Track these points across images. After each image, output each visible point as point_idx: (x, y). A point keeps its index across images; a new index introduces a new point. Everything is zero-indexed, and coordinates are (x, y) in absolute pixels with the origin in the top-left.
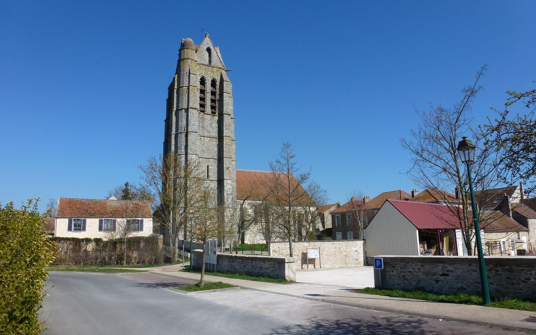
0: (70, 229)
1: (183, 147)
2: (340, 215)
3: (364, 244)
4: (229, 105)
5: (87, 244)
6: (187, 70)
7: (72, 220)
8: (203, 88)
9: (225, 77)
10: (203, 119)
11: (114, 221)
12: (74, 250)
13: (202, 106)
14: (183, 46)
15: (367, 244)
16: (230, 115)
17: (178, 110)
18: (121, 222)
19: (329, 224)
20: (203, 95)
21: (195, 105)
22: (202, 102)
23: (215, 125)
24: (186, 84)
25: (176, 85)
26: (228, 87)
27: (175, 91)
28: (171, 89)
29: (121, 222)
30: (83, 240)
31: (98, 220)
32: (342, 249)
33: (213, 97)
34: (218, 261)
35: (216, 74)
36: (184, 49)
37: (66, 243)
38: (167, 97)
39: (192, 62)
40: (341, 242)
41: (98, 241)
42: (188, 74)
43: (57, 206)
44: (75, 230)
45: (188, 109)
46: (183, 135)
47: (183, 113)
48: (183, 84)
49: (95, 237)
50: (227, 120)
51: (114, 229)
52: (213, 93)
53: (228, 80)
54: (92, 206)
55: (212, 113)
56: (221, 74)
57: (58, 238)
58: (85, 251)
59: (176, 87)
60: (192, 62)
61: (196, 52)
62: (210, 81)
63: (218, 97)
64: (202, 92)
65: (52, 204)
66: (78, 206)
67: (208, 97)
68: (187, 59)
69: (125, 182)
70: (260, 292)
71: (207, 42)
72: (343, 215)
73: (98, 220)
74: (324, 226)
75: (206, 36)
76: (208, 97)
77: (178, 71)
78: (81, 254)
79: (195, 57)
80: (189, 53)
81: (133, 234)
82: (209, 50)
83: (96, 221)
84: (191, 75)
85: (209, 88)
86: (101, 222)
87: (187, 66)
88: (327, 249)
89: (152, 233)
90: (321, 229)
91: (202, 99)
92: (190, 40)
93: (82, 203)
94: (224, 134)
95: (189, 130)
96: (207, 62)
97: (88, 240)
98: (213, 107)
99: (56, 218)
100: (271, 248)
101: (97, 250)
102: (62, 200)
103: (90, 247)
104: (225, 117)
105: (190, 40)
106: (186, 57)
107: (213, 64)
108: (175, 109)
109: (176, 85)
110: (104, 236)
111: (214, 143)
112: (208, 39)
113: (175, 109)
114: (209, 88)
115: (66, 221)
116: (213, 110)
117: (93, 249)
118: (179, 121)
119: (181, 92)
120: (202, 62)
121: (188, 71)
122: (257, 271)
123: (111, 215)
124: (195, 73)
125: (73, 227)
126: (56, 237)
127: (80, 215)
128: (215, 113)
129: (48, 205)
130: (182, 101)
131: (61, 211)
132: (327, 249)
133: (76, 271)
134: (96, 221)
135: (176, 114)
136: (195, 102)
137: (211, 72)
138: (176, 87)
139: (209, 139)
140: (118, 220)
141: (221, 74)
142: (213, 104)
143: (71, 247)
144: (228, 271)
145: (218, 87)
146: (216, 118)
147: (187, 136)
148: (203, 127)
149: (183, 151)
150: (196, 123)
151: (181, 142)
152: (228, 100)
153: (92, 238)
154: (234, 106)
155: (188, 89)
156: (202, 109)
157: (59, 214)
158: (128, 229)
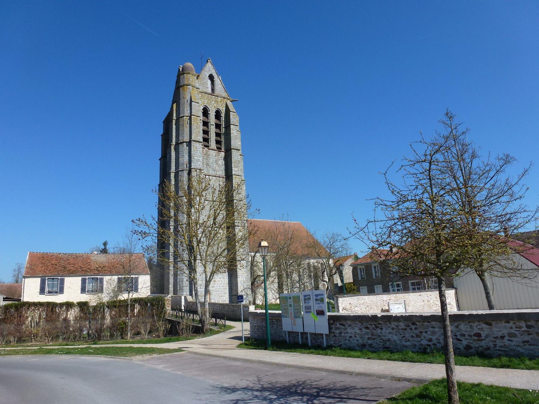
0: (42, 291)
2: (363, 267)
3: (456, 293)
4: (236, 141)
5: (68, 311)
7: (45, 280)
8: (206, 120)
9: (231, 108)
10: (207, 155)
11: (102, 280)
12: (49, 320)
13: (206, 140)
14: (181, 74)
15: (459, 292)
16: (239, 150)
17: (178, 144)
18: (110, 281)
19: (348, 277)
20: (206, 128)
21: (199, 137)
22: (206, 136)
23: (222, 162)
24: (187, 113)
25: (175, 115)
26: (234, 118)
27: (174, 122)
28: (167, 122)
29: (110, 281)
30: (61, 305)
31: (80, 279)
32: (431, 302)
33: (218, 131)
34: (330, 328)
37: (39, 310)
38: (161, 132)
39: (193, 89)
40: (366, 297)
41: (83, 305)
42: (189, 102)
43: (23, 271)
44: (49, 292)
45: (190, 142)
46: (185, 173)
47: (184, 148)
49: (79, 301)
50: (236, 156)
51: (101, 291)
52: (218, 126)
53: (234, 110)
54: (72, 261)
55: (218, 148)
56: (226, 104)
57: (27, 303)
58: (66, 320)
59: (174, 117)
60: (193, 89)
61: (197, 78)
63: (223, 130)
64: (205, 124)
65: (19, 269)
66: (54, 262)
67: (213, 130)
68: (188, 85)
69: (103, 241)
71: (209, 69)
72: (368, 267)
73: (80, 279)
74: (342, 281)
75: (207, 62)
76: (213, 130)
77: (177, 99)
78: (59, 324)
79: (197, 83)
80: (190, 78)
81: (124, 296)
82: (211, 77)
83: (77, 281)
84: (193, 103)
85: (212, 120)
86: (84, 282)
87: (187, 94)
88: (413, 303)
89: (149, 294)
90: (340, 284)
91: (206, 132)
92: (189, 64)
93: (58, 258)
94: (233, 172)
95: (193, 167)
96: (210, 91)
97: (69, 305)
98: (218, 142)
99: (24, 277)
100: (340, 304)
101: (81, 317)
102: (32, 255)
103: (72, 314)
104: (234, 152)
105: (189, 64)
107: (217, 92)
108: (174, 142)
109: (175, 115)
110: (92, 300)
113: (174, 142)
114: (212, 120)
115: (38, 281)
116: (219, 146)
117: (76, 318)
118: (180, 156)
119: (181, 123)
120: (204, 90)
121: (189, 99)
122: (465, 343)
123: (97, 272)
124: (198, 101)
125: (47, 290)
126: (24, 302)
127: (56, 273)
128: (221, 149)
129: (15, 270)
130: (183, 133)
131: (31, 269)
132: (413, 303)
133: (57, 353)
134: (77, 281)
135: (175, 149)
136: (198, 134)
137: (215, 101)
138: (174, 117)
139: (214, 178)
140: (106, 278)
141: (226, 104)
142: (218, 138)
143: (44, 315)
144: (364, 346)
145: (223, 119)
146: (223, 154)
147: (189, 173)
148: (208, 165)
150: (201, 159)
152: (235, 132)
153: (75, 302)
154: (243, 140)
155: (190, 119)
156: (206, 143)
157: (27, 273)
158: (120, 290)
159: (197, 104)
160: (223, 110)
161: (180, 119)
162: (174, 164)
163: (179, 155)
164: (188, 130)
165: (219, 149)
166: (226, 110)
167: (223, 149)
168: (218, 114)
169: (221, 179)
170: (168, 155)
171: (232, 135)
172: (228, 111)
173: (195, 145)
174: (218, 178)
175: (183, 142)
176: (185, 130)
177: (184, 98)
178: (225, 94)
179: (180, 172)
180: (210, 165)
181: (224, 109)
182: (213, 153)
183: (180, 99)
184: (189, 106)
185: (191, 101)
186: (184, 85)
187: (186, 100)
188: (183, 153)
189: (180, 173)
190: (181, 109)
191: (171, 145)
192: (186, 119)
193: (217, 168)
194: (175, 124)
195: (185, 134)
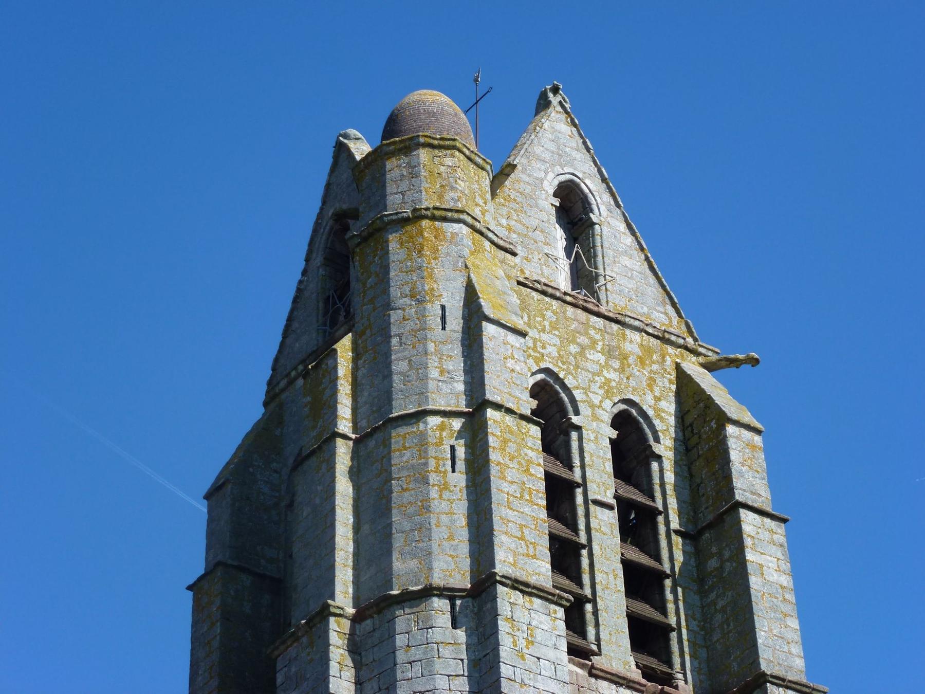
6: (452, 299)
17: (379, 607)
24: (448, 390)
35: (641, 375)
42: (455, 322)
52: (637, 524)
62: (607, 418)
63: (674, 554)
68: (442, 215)
70: (508, 246)
71: (555, 150)
82: (572, 210)
84: (489, 329)
92: (435, 99)
105: (435, 99)
106: (428, 201)
108: (344, 596)
114: (599, 476)
119: (402, 457)
121: (455, 304)
124: (520, 324)
130: (424, 530)
135: (354, 648)
137: (609, 352)
156: (581, 295)
159: (512, 338)
160: (663, 414)
161: (398, 435)
164: (461, 508)
166: (681, 416)
168: (630, 431)
171: (755, 582)
172: (701, 424)
173: (521, 615)
175: (428, 592)
176: (439, 505)
178: (662, 316)
181: (669, 406)
183: (388, 306)
184: (457, 350)
186: (418, 216)
190: (399, 366)
192: (443, 434)
194: (354, 474)
195: (439, 534)
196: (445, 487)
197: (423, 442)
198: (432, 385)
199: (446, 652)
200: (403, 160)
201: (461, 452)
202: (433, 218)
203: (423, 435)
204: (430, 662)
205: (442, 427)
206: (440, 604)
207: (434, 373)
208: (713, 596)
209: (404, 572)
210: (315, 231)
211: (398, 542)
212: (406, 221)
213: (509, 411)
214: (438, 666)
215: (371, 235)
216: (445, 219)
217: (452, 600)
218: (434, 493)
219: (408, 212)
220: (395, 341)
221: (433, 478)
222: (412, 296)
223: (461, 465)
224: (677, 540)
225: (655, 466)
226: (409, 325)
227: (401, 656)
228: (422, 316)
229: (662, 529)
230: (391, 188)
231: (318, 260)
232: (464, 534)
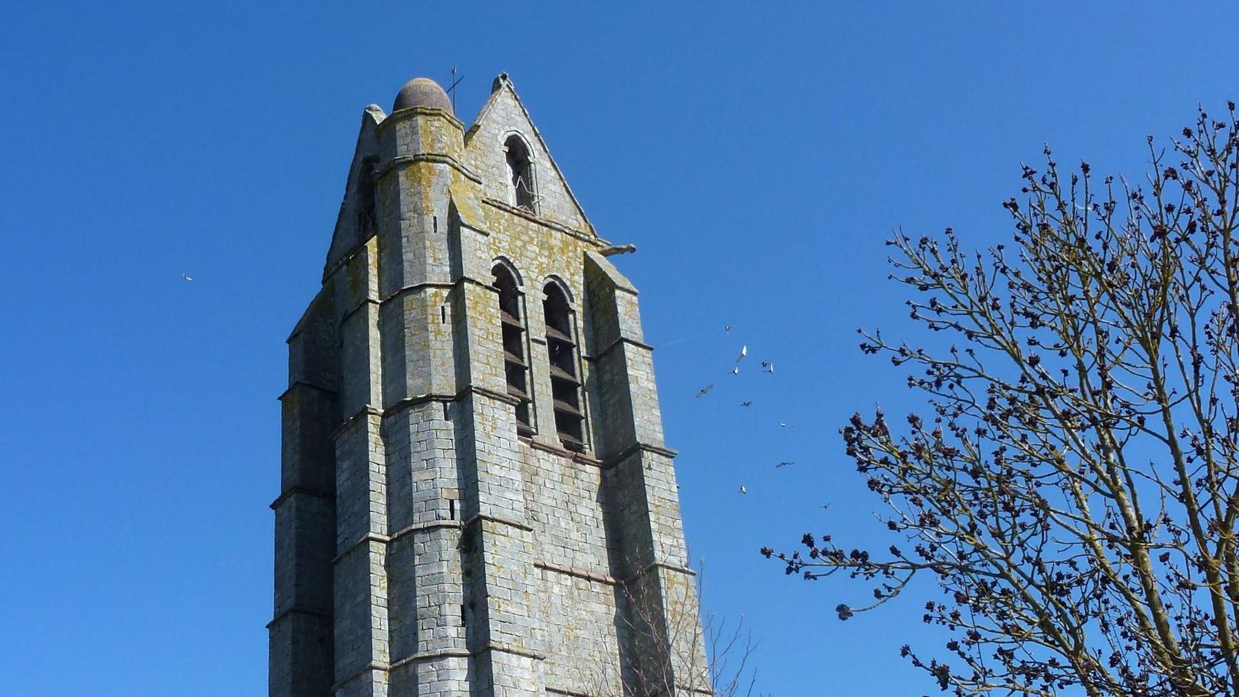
1: (453, 612)
23: (591, 511)
24: (440, 272)
36: (411, 115)
42: (443, 228)
46: (449, 543)
48: (423, 274)
50: (661, 482)
52: (560, 353)
55: (567, 445)
63: (583, 371)
68: (433, 159)
71: (505, 116)
75: (497, 86)
82: (517, 154)
84: (465, 232)
92: (427, 84)
98: (567, 423)
105: (427, 84)
106: (423, 151)
108: (376, 402)
111: (600, 609)
112: (511, 102)
118: (415, 461)
119: (411, 314)
121: (442, 215)
124: (485, 228)
128: (580, 449)
130: (426, 360)
135: (384, 433)
137: (542, 245)
139: (568, 581)
145: (578, 320)
147: (471, 544)
149: (452, 632)
151: (438, 579)
152: (640, 371)
159: (479, 237)
161: (408, 299)
162: (383, 500)
163: (407, 457)
165: (574, 449)
166: (587, 285)
167: (590, 453)
169: (597, 587)
170: (345, 465)
174: (583, 583)
175: (429, 398)
176: (435, 344)
177: (419, 212)
178: (575, 222)
179: (418, 538)
180: (542, 516)
181: (580, 279)
182: (552, 466)
183: (400, 218)
185: (455, 223)
187: (429, 220)
188: (431, 448)
189: (419, 542)
190: (407, 256)
191: (365, 412)
192: (437, 299)
193: (575, 535)
194: (381, 325)
195: (435, 362)
196: (438, 333)
197: (424, 306)
198: (429, 268)
199: (441, 435)
200: (407, 124)
201: (448, 311)
202: (427, 160)
203: (424, 300)
204: (432, 442)
205: (436, 295)
206: (437, 406)
207: (430, 261)
208: (607, 396)
209: (414, 386)
210: (353, 166)
211: (410, 367)
212: (410, 162)
213: (479, 284)
214: (437, 443)
215: (387, 172)
216: (435, 161)
217: (445, 403)
218: (432, 337)
219: (411, 157)
220: (404, 240)
221: (431, 327)
222: (415, 211)
223: (448, 318)
224: (585, 363)
225: (571, 316)
226: (413, 230)
227: (413, 438)
228: (421, 223)
229: (576, 356)
230: (399, 142)
231: (354, 189)
232: (452, 361)
